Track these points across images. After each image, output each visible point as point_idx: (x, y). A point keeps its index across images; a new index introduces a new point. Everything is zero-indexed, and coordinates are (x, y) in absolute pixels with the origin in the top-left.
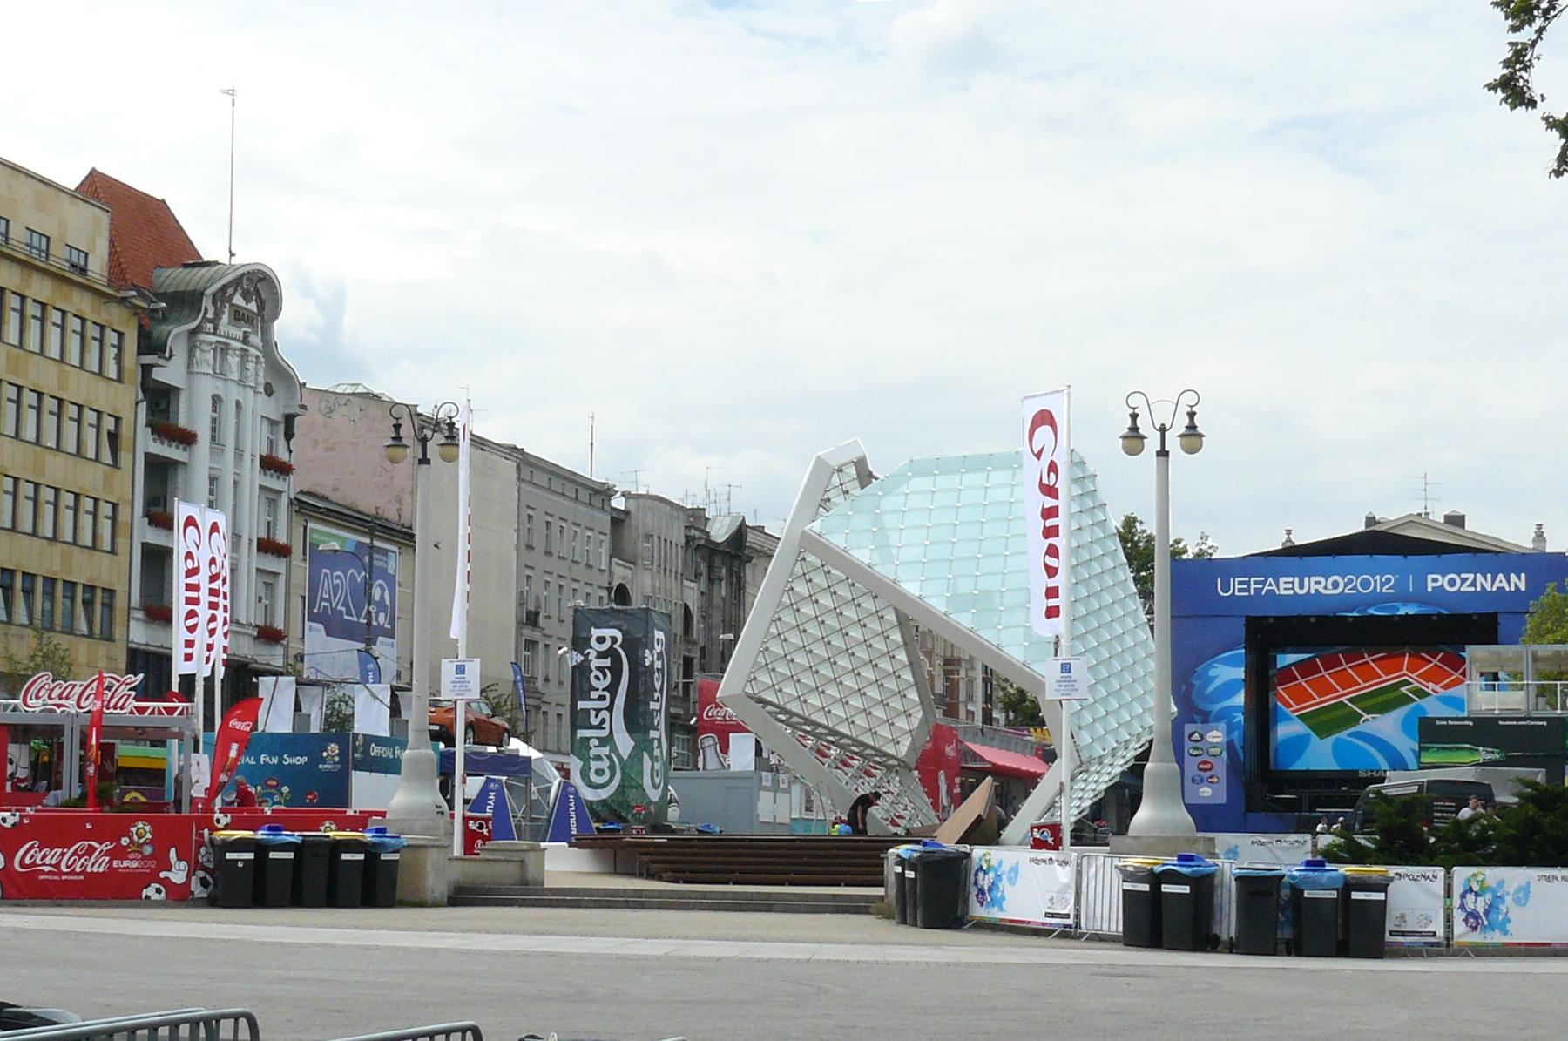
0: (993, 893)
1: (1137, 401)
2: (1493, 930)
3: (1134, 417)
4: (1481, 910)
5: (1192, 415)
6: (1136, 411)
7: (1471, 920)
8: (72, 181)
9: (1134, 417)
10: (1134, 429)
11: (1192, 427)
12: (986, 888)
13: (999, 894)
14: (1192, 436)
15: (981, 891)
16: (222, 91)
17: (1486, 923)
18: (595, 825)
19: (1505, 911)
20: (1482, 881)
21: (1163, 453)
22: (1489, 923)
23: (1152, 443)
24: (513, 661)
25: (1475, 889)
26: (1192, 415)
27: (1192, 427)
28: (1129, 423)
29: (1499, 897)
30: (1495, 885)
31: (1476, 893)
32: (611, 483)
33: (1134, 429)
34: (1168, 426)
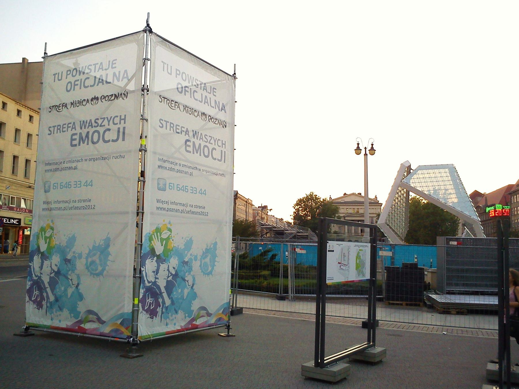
0: (60, 288)
1: (359, 140)
2: (61, 309)
3: (358, 144)
4: (162, 284)
5: (372, 145)
6: (359, 143)
7: (150, 300)
8: (343, 195)
9: (358, 144)
10: (358, 147)
11: (372, 148)
12: (46, 279)
13: (186, 291)
14: (372, 151)
15: (38, 284)
16: (237, 102)
17: (168, 302)
18: (10, 252)
19: (190, 283)
20: (168, 239)
21: (366, 154)
22: (173, 303)
23: (363, 152)
24: (91, 186)
25: (158, 253)
26: (372, 145)
27: (372, 148)
28: (357, 146)
29: (186, 263)
30: (182, 247)
31: (158, 257)
32: (308, 194)
33: (358, 147)
34: (367, 147)
